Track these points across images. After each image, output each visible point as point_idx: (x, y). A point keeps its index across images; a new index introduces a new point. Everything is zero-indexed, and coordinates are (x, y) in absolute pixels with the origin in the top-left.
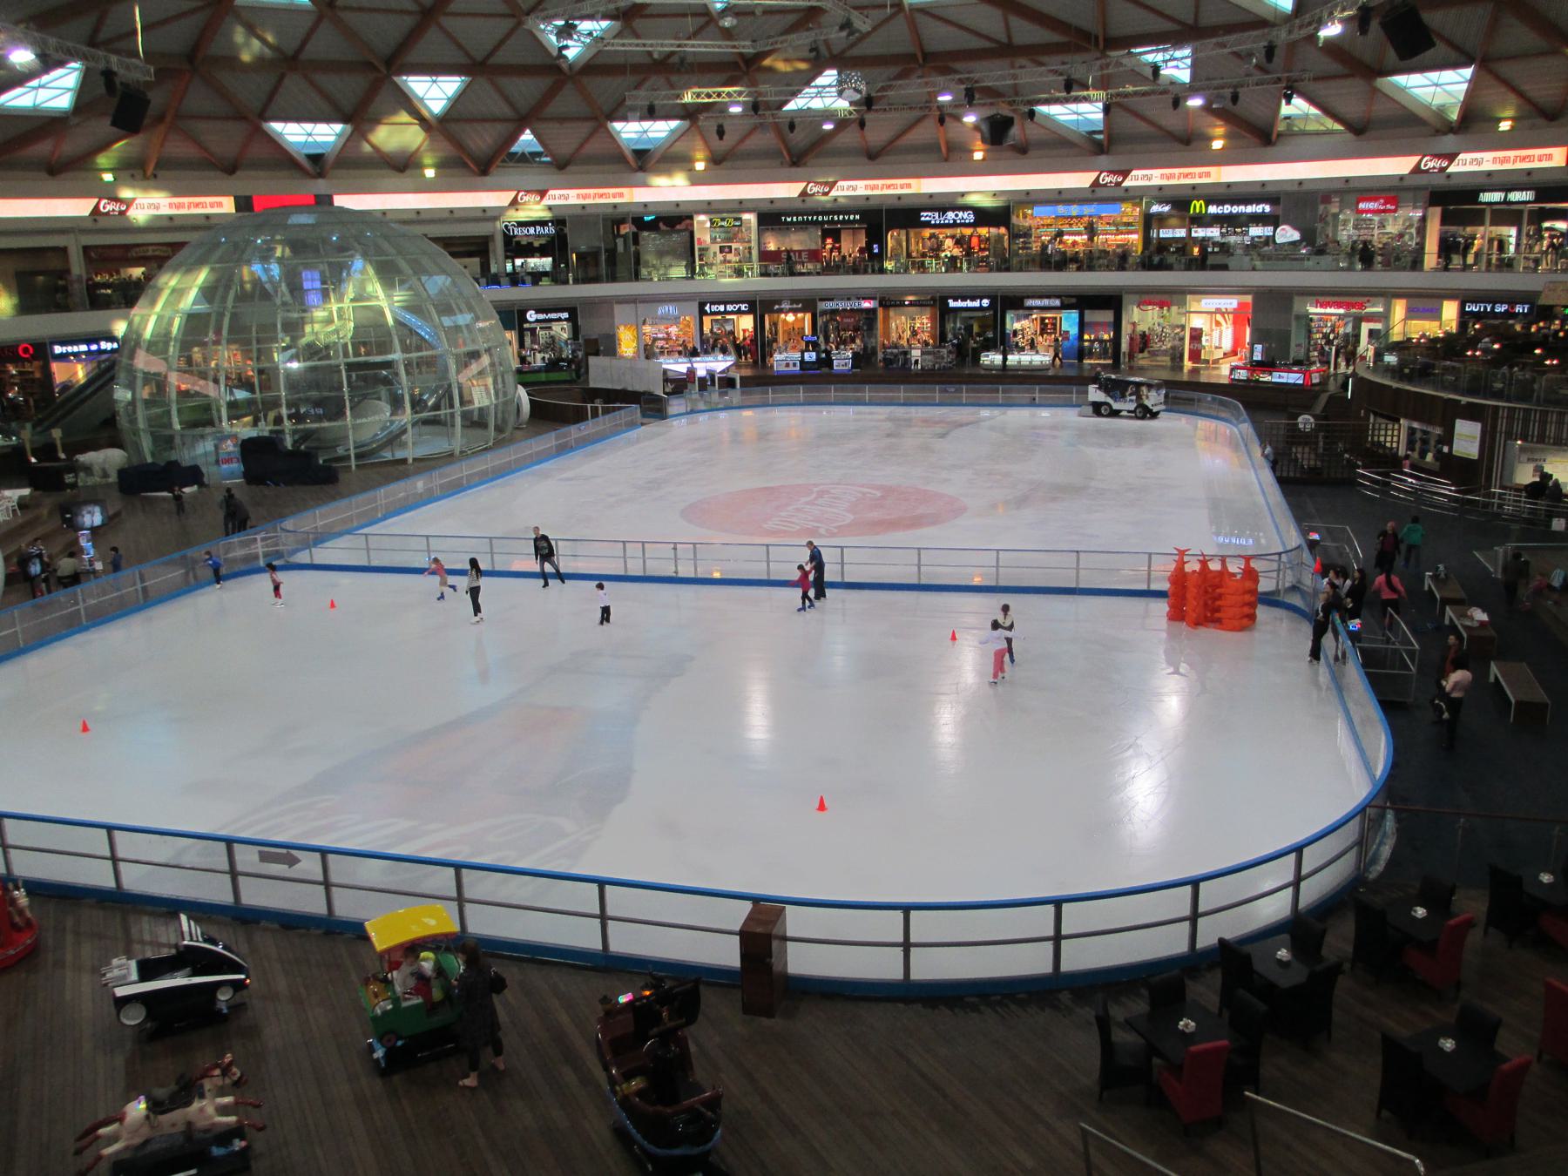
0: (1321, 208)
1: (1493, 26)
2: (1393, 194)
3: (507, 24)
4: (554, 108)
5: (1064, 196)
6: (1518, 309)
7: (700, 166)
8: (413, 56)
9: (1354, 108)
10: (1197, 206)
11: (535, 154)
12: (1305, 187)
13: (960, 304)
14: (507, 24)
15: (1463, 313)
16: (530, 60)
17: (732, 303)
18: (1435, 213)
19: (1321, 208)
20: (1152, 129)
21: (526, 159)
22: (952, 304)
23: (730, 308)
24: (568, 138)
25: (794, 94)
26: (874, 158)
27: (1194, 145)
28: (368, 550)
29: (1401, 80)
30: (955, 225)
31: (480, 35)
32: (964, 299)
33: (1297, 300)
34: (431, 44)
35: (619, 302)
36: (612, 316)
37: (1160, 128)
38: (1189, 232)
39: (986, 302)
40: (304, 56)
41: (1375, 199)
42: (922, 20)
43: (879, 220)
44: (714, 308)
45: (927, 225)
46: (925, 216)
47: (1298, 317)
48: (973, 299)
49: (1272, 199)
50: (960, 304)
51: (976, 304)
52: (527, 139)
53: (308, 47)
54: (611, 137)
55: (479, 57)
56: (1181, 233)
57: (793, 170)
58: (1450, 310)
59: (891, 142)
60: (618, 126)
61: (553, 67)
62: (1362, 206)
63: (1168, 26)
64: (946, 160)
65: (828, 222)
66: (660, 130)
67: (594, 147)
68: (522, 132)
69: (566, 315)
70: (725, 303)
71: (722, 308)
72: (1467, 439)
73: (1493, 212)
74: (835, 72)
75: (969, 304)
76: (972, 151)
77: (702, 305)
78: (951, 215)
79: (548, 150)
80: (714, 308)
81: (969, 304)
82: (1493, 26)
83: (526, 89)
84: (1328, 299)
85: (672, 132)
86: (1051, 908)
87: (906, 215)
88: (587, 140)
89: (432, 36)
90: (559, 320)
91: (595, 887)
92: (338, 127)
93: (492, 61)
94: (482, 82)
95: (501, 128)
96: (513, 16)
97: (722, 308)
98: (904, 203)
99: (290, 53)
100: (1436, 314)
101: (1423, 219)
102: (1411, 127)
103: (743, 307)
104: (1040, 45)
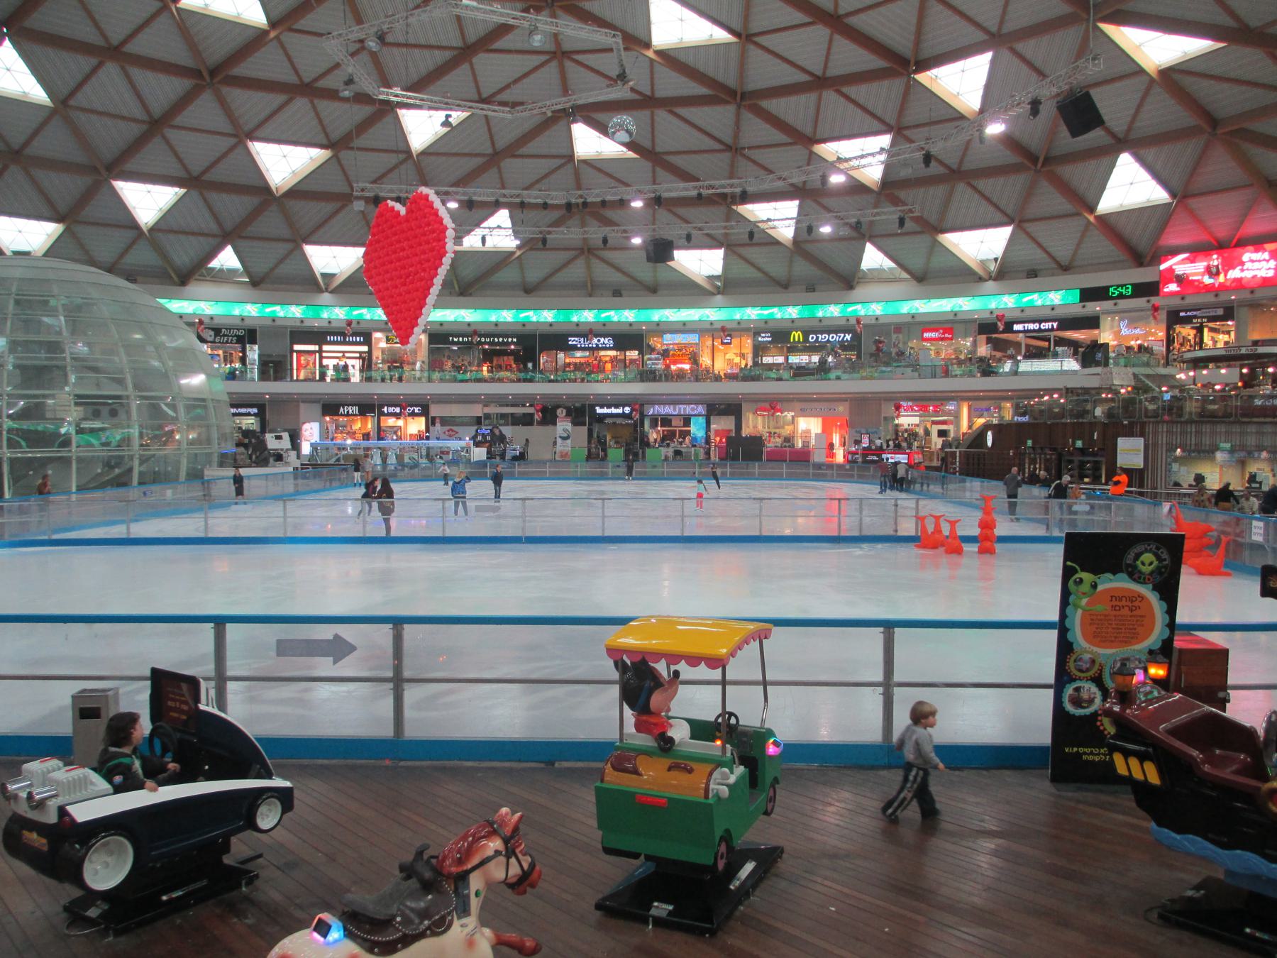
0: (894, 336)
1: (1029, 194)
2: (949, 326)
3: (224, 143)
4: (258, 227)
5: (688, 327)
8: (130, 166)
9: (917, 263)
11: (233, 272)
13: (605, 411)
14: (233, 141)
19: (894, 336)
20: (759, 275)
21: (223, 277)
22: (599, 410)
24: (267, 256)
26: (530, 291)
31: (198, 152)
32: (609, 407)
34: (154, 153)
35: (304, 401)
36: (298, 413)
37: (765, 273)
38: (787, 359)
39: (627, 410)
40: (29, 151)
43: (529, 348)
44: (391, 410)
45: (575, 348)
46: (573, 341)
47: (885, 418)
48: (617, 406)
50: (605, 411)
51: (619, 411)
52: (227, 259)
53: (35, 143)
55: (196, 169)
56: (780, 360)
57: (462, 298)
59: (546, 279)
62: (926, 335)
64: (590, 295)
65: (489, 343)
67: (287, 268)
69: (255, 410)
71: (398, 410)
75: (614, 411)
79: (247, 270)
80: (391, 410)
81: (614, 411)
82: (1029, 194)
83: (233, 207)
87: (556, 340)
88: (281, 261)
89: (156, 144)
90: (249, 414)
93: (207, 177)
95: (206, 243)
96: (235, 136)
98: (555, 329)
99: (17, 147)
103: (417, 410)
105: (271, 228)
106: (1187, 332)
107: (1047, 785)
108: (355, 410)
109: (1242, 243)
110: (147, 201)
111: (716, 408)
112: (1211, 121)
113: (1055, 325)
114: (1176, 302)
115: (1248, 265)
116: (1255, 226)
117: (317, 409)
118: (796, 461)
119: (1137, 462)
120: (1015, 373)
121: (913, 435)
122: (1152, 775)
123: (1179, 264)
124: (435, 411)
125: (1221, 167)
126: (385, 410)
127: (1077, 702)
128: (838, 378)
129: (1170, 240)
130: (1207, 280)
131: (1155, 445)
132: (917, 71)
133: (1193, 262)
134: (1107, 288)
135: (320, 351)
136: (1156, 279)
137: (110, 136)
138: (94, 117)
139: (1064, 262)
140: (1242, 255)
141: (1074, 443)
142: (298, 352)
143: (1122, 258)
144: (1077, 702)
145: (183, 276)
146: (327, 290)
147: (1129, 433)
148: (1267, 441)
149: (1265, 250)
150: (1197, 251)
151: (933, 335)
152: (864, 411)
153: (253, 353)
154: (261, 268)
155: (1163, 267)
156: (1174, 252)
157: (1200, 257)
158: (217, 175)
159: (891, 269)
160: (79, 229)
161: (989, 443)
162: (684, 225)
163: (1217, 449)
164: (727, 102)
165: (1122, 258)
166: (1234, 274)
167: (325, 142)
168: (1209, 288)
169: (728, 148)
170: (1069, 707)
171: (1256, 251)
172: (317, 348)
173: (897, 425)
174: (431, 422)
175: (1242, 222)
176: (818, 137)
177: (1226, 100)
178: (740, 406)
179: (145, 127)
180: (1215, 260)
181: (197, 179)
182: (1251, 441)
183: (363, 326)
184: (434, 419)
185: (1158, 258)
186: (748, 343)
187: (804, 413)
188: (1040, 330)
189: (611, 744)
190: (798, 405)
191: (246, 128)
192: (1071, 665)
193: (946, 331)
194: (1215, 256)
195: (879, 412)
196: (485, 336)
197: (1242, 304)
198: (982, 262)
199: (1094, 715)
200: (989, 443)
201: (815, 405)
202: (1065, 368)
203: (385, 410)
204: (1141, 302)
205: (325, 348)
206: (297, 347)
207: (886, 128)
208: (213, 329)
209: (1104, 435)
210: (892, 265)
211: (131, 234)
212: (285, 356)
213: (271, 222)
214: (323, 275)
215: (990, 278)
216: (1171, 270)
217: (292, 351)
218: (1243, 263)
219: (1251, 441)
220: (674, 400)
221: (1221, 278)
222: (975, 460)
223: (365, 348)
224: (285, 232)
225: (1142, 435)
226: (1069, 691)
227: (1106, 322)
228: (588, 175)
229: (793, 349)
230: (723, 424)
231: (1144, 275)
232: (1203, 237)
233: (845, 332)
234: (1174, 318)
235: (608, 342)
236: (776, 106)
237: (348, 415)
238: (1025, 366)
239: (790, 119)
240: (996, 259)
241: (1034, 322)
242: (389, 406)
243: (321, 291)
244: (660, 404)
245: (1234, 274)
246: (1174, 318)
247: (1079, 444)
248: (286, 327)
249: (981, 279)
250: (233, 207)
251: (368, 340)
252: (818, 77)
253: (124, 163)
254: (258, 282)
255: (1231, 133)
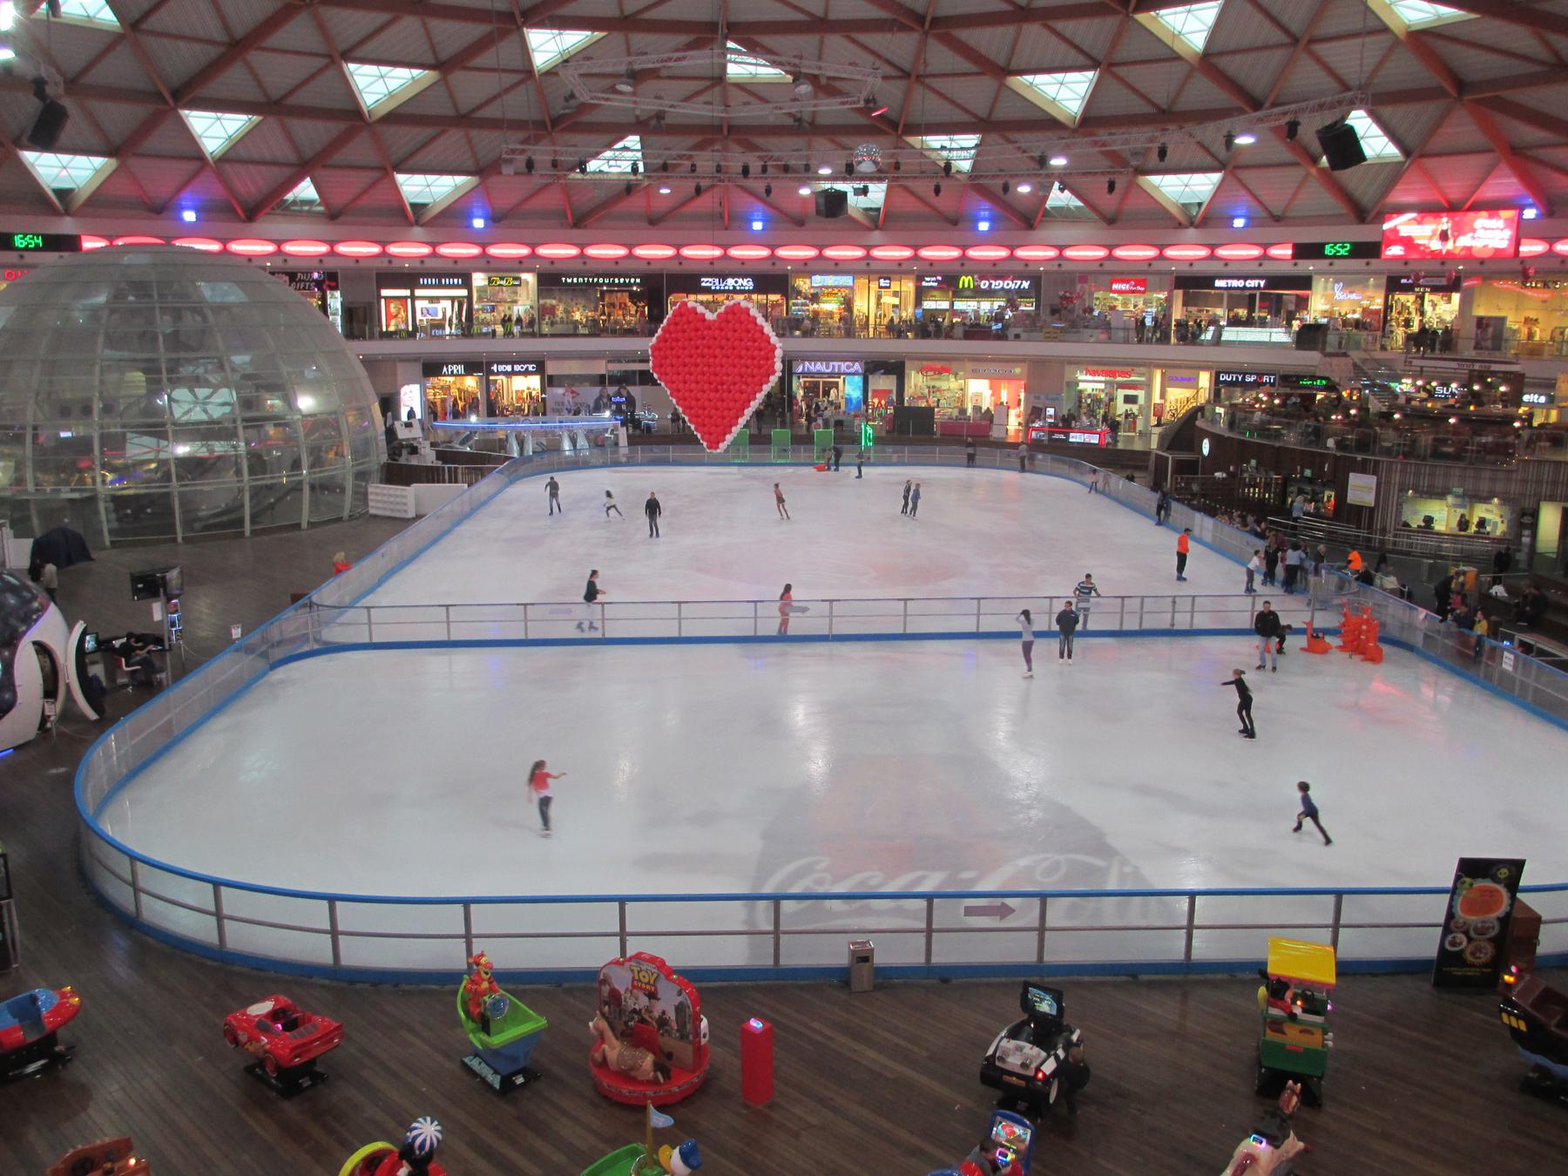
0: (1079, 287)
3: (319, 62)
6: (1266, 379)
7: (479, 223)
9: (1108, 203)
10: (966, 281)
11: (310, 202)
12: (362, 264)
14: (319, 62)
15: (1217, 382)
16: (337, 105)
17: (519, 363)
18: (1179, 294)
19: (1079, 287)
21: (300, 211)
23: (517, 368)
24: (348, 185)
25: (595, 155)
26: (657, 222)
27: (961, 225)
28: (448, 622)
29: (1155, 179)
30: (735, 291)
33: (1068, 368)
34: (234, 78)
36: (395, 375)
38: (952, 304)
41: (1127, 282)
42: (734, 92)
45: (707, 290)
46: (706, 282)
47: (1068, 384)
49: (1036, 280)
52: (306, 190)
54: (395, 187)
55: (275, 94)
56: (945, 305)
58: (1205, 379)
60: (401, 178)
61: (351, 113)
62: (1115, 286)
63: (965, 118)
66: (1198, 186)
68: (301, 178)
70: (513, 363)
71: (509, 368)
72: (1362, 489)
73: (1230, 296)
74: (637, 138)
76: (752, 221)
77: (1218, 374)
78: (731, 282)
80: (501, 368)
83: (312, 133)
84: (1101, 368)
85: (457, 188)
86: (1331, 899)
91: (325, 903)
92: (98, 161)
94: (272, 120)
97: (509, 368)
100: (1192, 382)
101: (1169, 300)
102: (1167, 222)
103: (531, 367)
104: (694, 126)
105: (356, 154)
106: (1408, 299)
107: (1427, 987)
108: (461, 368)
109: (1477, 207)
110: (214, 130)
111: (874, 366)
112: (1461, 85)
113: (1262, 283)
114: (1398, 268)
115: (1479, 233)
116: (1490, 191)
117: (418, 368)
118: (972, 439)
119: (1368, 499)
120: (1217, 341)
121: (1096, 400)
122: (1523, 1026)
123: (1404, 224)
124: (552, 368)
125: (1463, 128)
126: (495, 368)
127: (1453, 944)
128: (1017, 337)
129: (1398, 196)
130: (1436, 245)
131: (1388, 483)
132: (1138, 9)
133: (1420, 223)
134: (1322, 246)
135: (413, 298)
136: (1377, 239)
137: (180, 60)
138: (166, 41)
139: (1277, 212)
140: (1473, 221)
141: (1302, 472)
142: (387, 298)
143: (1344, 211)
144: (1453, 944)
145: (250, 210)
146: (417, 223)
147: (1363, 468)
148: (1499, 487)
149: (1499, 217)
150: (1428, 210)
151: (1124, 287)
152: (1044, 379)
153: (335, 301)
154: (339, 200)
155: (1386, 226)
156: (1400, 210)
157: (1429, 218)
158: (304, 98)
159: (1077, 208)
160: (133, 162)
161: (1206, 451)
162: (840, 152)
163: (1450, 493)
164: (911, 29)
165: (1344, 211)
166: (1464, 241)
167: (432, 61)
168: (1435, 255)
169: (906, 75)
170: (1448, 947)
171: (1491, 217)
172: (407, 293)
173: (1081, 392)
174: (549, 382)
175: (1478, 186)
176: (1013, 66)
177: (1475, 64)
178: (903, 364)
179: (221, 50)
180: (1445, 223)
181: (278, 103)
182: (1484, 487)
183: (460, 265)
184: (550, 377)
185: (1382, 216)
186: (909, 287)
187: (976, 375)
188: (1245, 288)
189: (1316, 1051)
190: (970, 365)
191: (343, 47)
192: (1452, 925)
193: (1138, 283)
194: (1445, 220)
195: (1062, 375)
196: (604, 276)
197: (1470, 275)
198: (1184, 205)
199: (1462, 951)
200: (1206, 451)
201: (985, 366)
202: (1274, 339)
203: (495, 368)
204: (1359, 264)
205: (418, 292)
206: (385, 292)
207: (1090, 63)
208: (287, 274)
209: (1334, 470)
210: (1080, 204)
211: (192, 166)
212: (370, 305)
213: (360, 150)
214: (413, 205)
215: (1192, 224)
216: (1395, 230)
217: (379, 297)
218: (1474, 230)
219: (1484, 487)
220: (827, 358)
221: (1450, 245)
222: (1189, 474)
223: (464, 292)
224: (372, 158)
225: (1374, 473)
226: (1450, 938)
227: (1319, 285)
228: (736, 97)
229: (959, 294)
230: (885, 383)
231: (1364, 234)
232: (1431, 196)
233: (1022, 278)
234: (1394, 285)
235: (747, 284)
236: (968, 35)
237: (452, 374)
238: (1230, 334)
239: (983, 50)
240: (1200, 204)
241: (1238, 278)
242: (499, 363)
243: (411, 225)
244: (810, 360)
245: (1464, 241)
246: (1394, 285)
247: (1308, 473)
248: (370, 269)
249: (1180, 225)
250: (312, 133)
251: (467, 284)
252: (1021, 8)
253: (197, 90)
254: (334, 214)
255: (1477, 101)
